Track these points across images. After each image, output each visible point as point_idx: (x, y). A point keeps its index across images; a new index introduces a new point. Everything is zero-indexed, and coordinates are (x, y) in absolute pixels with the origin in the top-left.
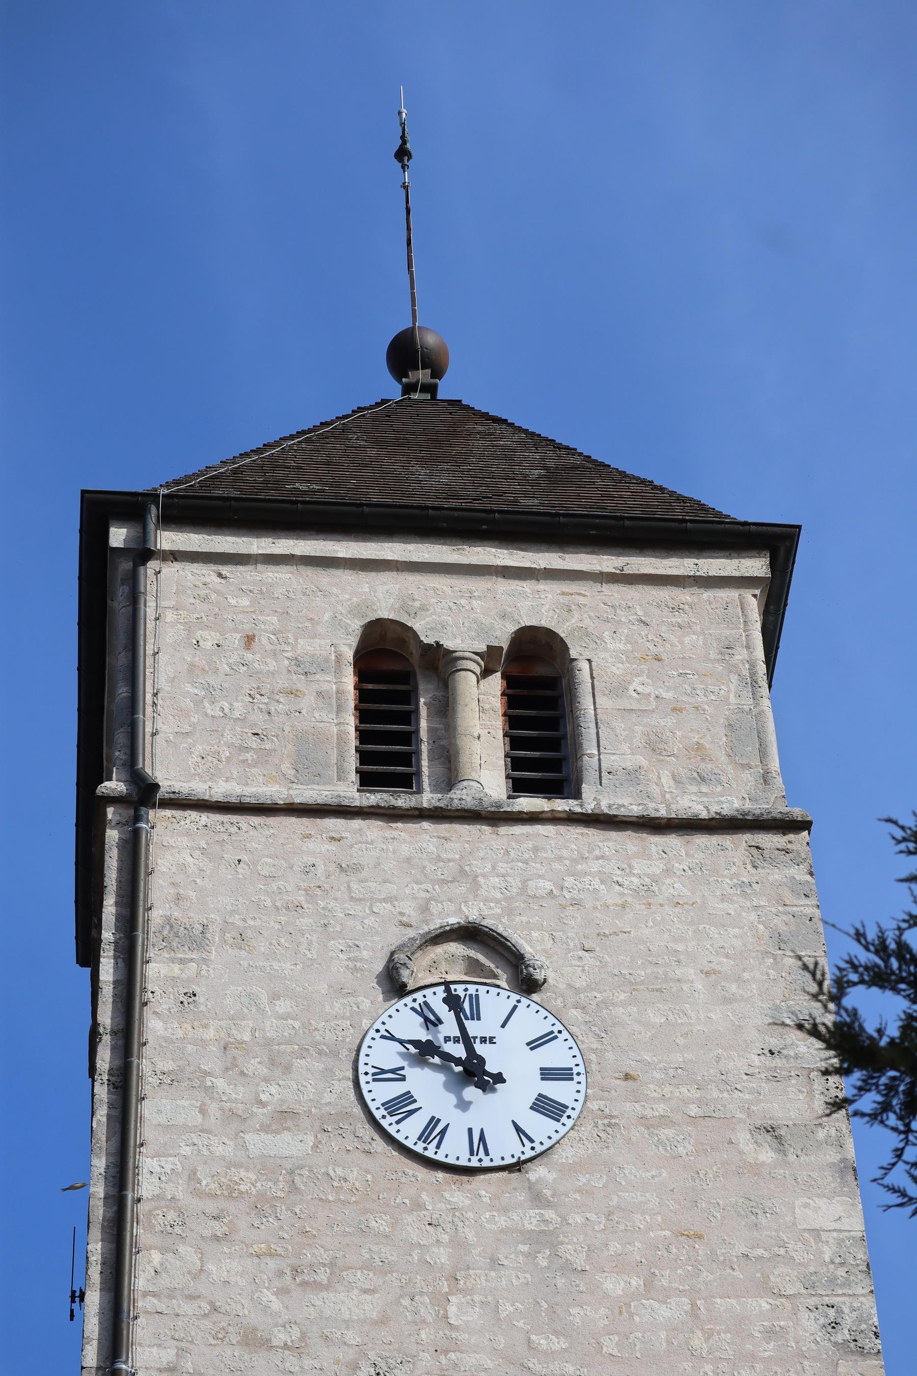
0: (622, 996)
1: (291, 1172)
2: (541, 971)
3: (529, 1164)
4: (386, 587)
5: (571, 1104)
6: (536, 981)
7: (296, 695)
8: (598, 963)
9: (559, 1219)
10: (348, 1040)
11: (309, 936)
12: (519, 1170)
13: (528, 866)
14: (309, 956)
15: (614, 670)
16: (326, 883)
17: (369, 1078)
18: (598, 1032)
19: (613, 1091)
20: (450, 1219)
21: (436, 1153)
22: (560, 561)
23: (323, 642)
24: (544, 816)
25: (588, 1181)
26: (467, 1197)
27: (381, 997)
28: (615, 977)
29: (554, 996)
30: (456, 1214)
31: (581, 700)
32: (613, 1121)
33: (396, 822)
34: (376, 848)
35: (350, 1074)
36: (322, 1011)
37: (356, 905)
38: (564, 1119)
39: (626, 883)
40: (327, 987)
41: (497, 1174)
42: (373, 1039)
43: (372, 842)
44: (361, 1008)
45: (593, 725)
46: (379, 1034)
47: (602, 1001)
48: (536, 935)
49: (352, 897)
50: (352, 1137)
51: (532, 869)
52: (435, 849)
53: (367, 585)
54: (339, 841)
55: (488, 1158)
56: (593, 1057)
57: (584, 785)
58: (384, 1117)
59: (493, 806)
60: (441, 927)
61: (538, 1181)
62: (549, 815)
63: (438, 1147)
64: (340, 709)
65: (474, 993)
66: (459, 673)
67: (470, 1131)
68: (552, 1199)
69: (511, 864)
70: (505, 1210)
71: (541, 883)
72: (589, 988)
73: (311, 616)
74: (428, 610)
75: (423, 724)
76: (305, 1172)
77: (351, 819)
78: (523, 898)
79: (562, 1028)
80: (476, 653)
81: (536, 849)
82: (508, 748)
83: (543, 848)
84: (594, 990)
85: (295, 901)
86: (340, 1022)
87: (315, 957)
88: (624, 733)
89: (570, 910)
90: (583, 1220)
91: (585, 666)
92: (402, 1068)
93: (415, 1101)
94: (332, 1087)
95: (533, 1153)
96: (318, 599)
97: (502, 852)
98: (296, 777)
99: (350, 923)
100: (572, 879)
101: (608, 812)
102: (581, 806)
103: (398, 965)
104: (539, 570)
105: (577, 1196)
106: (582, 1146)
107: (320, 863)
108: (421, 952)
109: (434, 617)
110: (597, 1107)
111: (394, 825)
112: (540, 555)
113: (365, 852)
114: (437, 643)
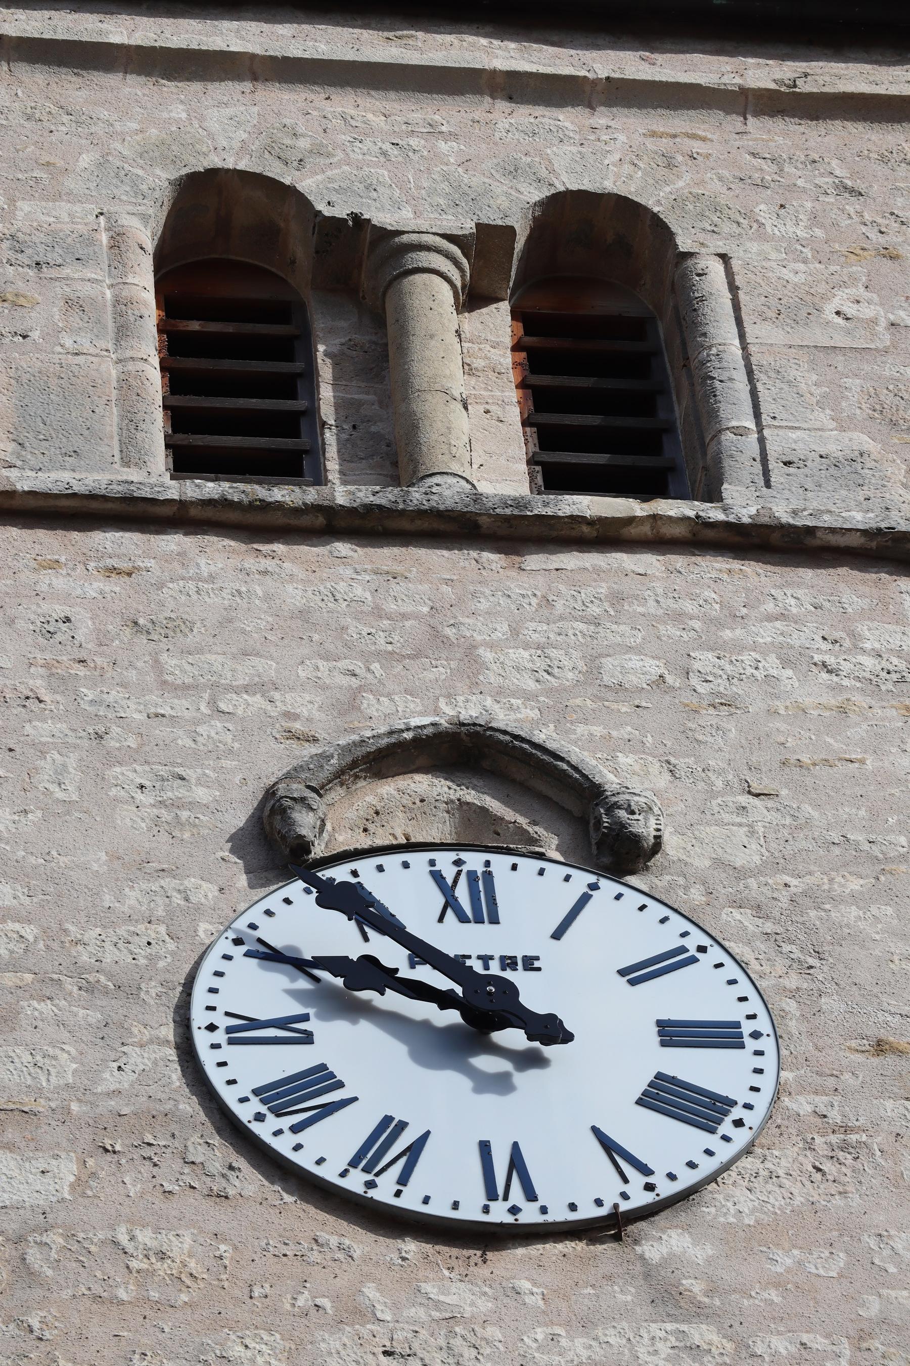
0: (855, 885)
1: (19, 1240)
2: (646, 819)
3: (642, 1225)
4: (230, 111)
5: (742, 1095)
6: (636, 839)
7: (14, 304)
8: (788, 821)
9: (729, 1346)
10: (161, 964)
11: (57, 756)
12: (617, 1238)
13: (600, 629)
14: (60, 795)
15: (786, 274)
16: (101, 654)
17: (220, 1037)
18: (797, 954)
19: (847, 1076)
20: (442, 1342)
21: (398, 1194)
22: (645, 66)
23: (78, 208)
24: (633, 531)
25: (800, 1263)
26: (485, 1294)
27: (242, 880)
28: (832, 847)
29: (681, 881)
30: (457, 1329)
31: (710, 329)
32: (853, 1138)
33: (270, 541)
34: (221, 589)
35: (168, 1032)
36: (94, 906)
37: (178, 698)
38: (726, 1127)
39: (846, 667)
40: (104, 857)
41: (560, 1246)
42: (228, 958)
43: (212, 578)
44: (193, 899)
45: (740, 376)
46: (243, 949)
47: (805, 894)
48: (630, 761)
49: (165, 682)
50: (178, 1165)
51: (609, 635)
52: (368, 595)
53: (181, 107)
54: (129, 574)
55: (536, 1206)
56: (791, 1006)
57: (725, 486)
58: (260, 1117)
59: (507, 506)
60: (391, 733)
61: (665, 1261)
62: (646, 530)
63: (403, 1180)
64: (123, 332)
65: (480, 869)
66: (411, 278)
67: (485, 1148)
68: (706, 1300)
69: (560, 624)
70: (586, 1324)
71: (634, 662)
72: (775, 865)
73: (45, 158)
74: (329, 155)
75: (326, 393)
76: (56, 1239)
77: (158, 532)
78: (591, 690)
79: (706, 941)
80: (451, 238)
81: (617, 598)
82: (533, 448)
83: (636, 597)
84: (784, 871)
85: (21, 688)
86: (140, 928)
87: (75, 797)
88: (817, 391)
89: (709, 717)
90: (793, 1349)
91: (716, 269)
92: (305, 1018)
93: (340, 1085)
94: (124, 1060)
95: (648, 1198)
96: (63, 128)
97: (534, 601)
98: (19, 456)
99: (161, 731)
100: (710, 655)
101: (791, 521)
102: (725, 510)
103: (288, 803)
104: (595, 82)
105: (774, 1295)
106: (777, 1189)
107: (80, 614)
108: (341, 791)
109: (346, 168)
110: (809, 1109)
111: (265, 548)
112: (595, 54)
113: (195, 597)
114: (356, 217)
